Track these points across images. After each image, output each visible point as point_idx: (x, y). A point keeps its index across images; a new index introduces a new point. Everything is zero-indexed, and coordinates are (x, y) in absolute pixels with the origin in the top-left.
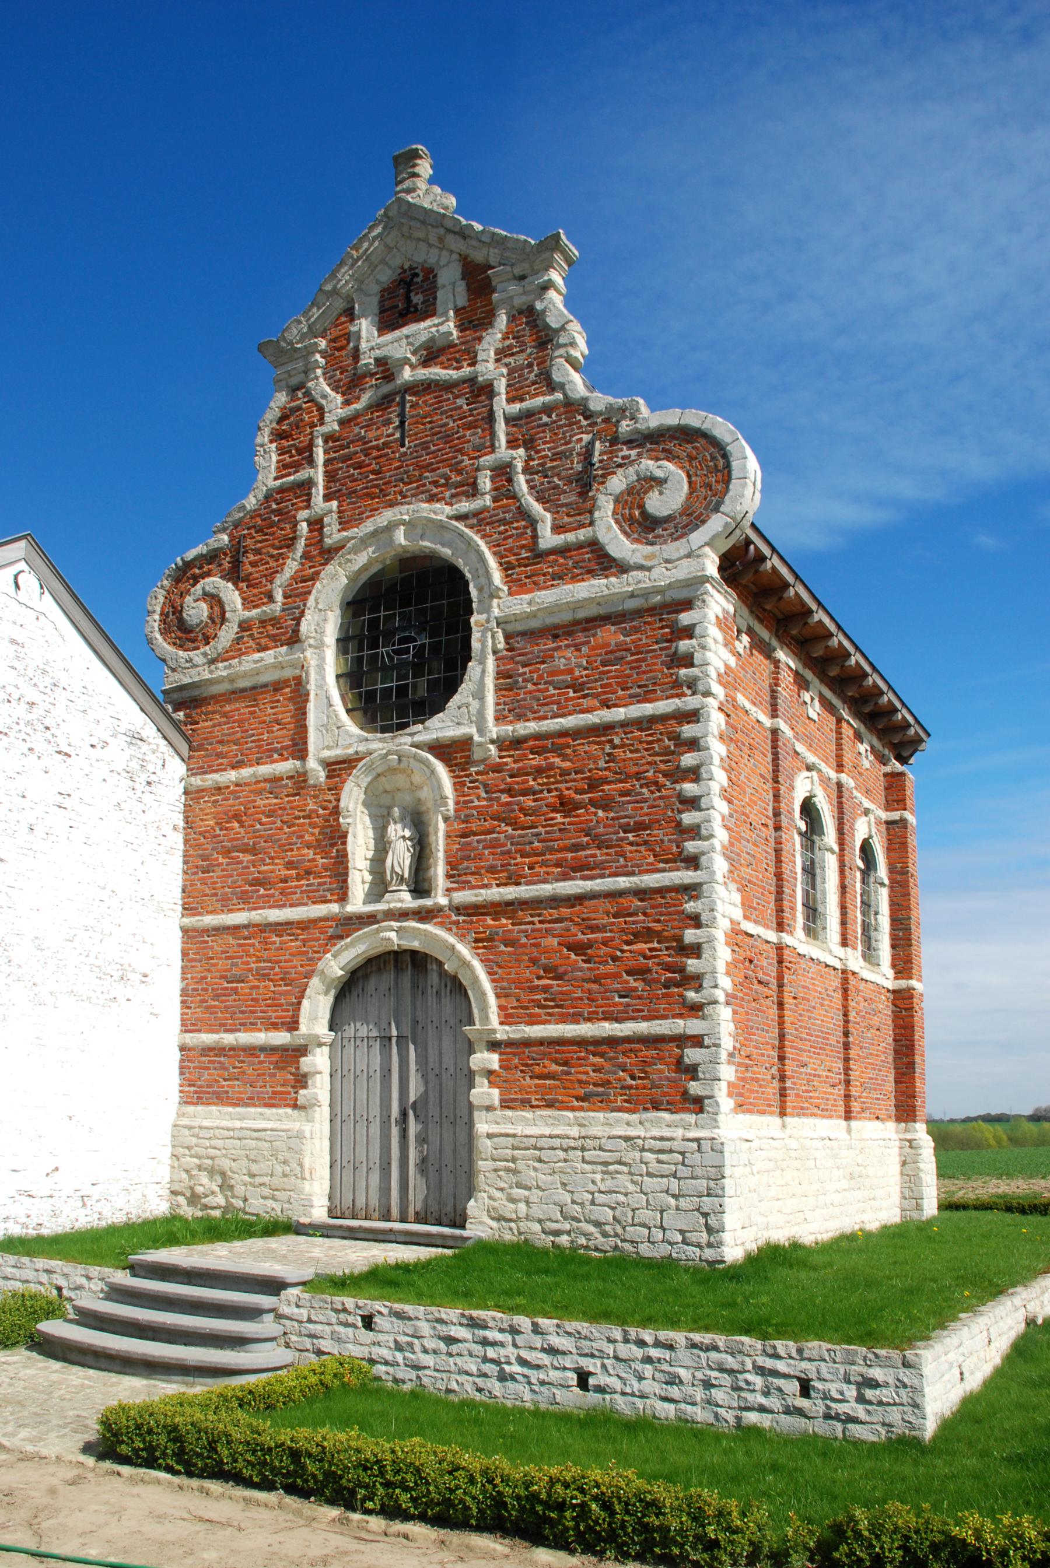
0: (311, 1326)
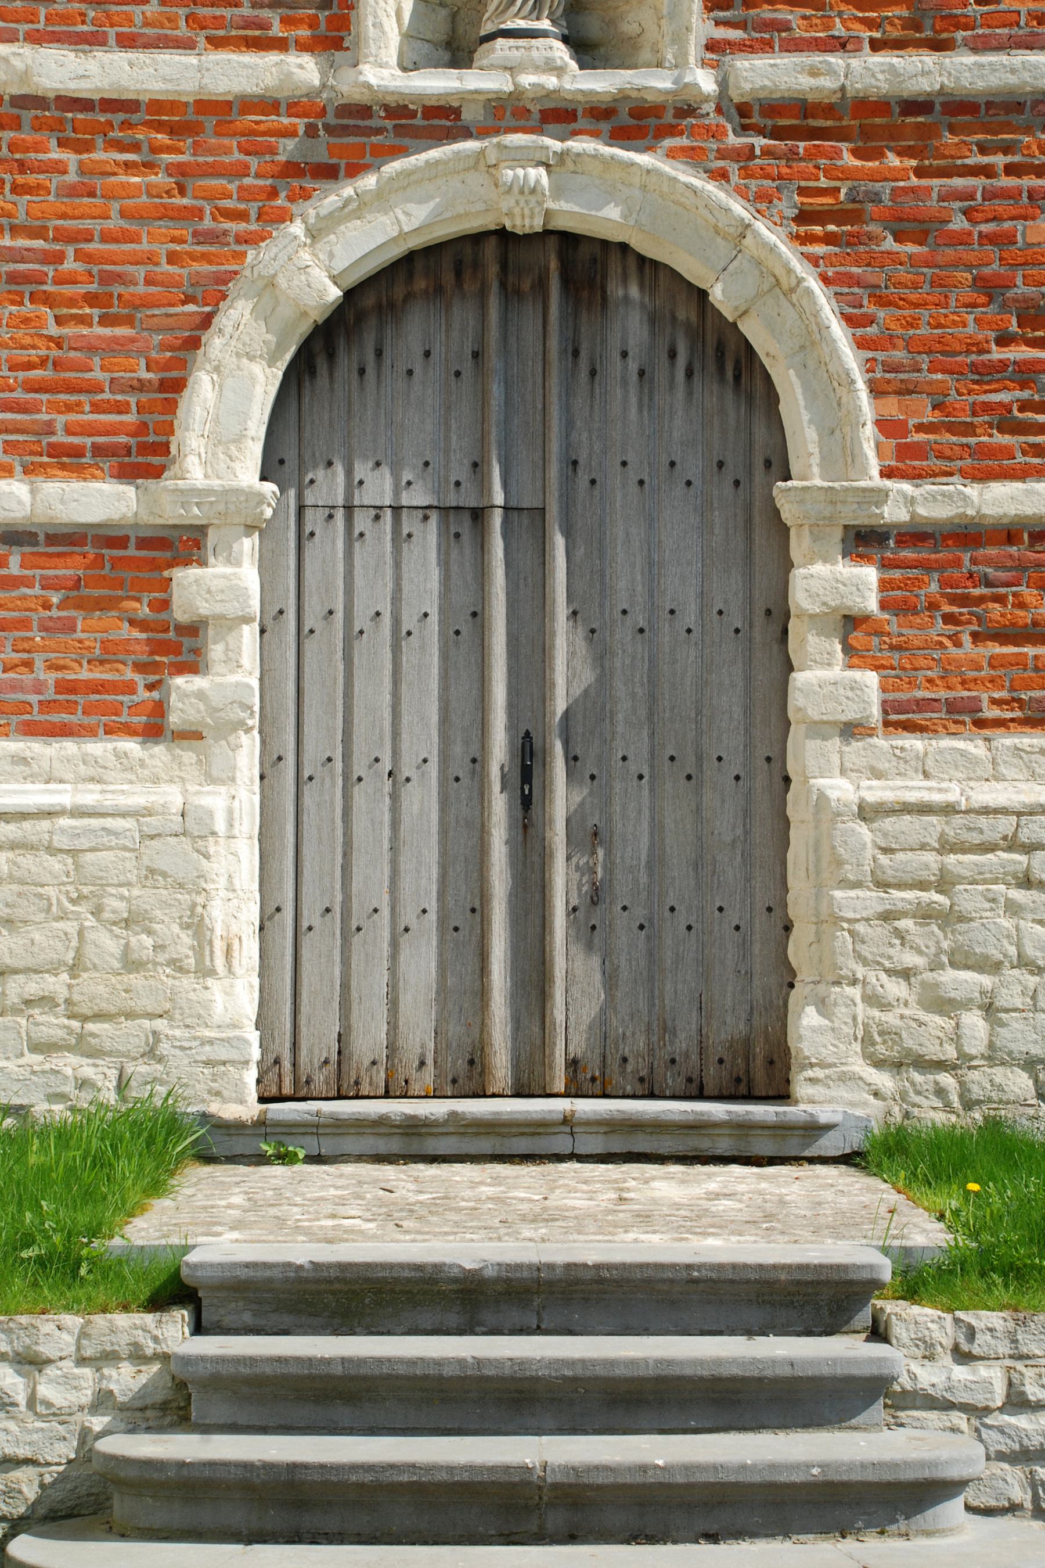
0: (1022, 1421)
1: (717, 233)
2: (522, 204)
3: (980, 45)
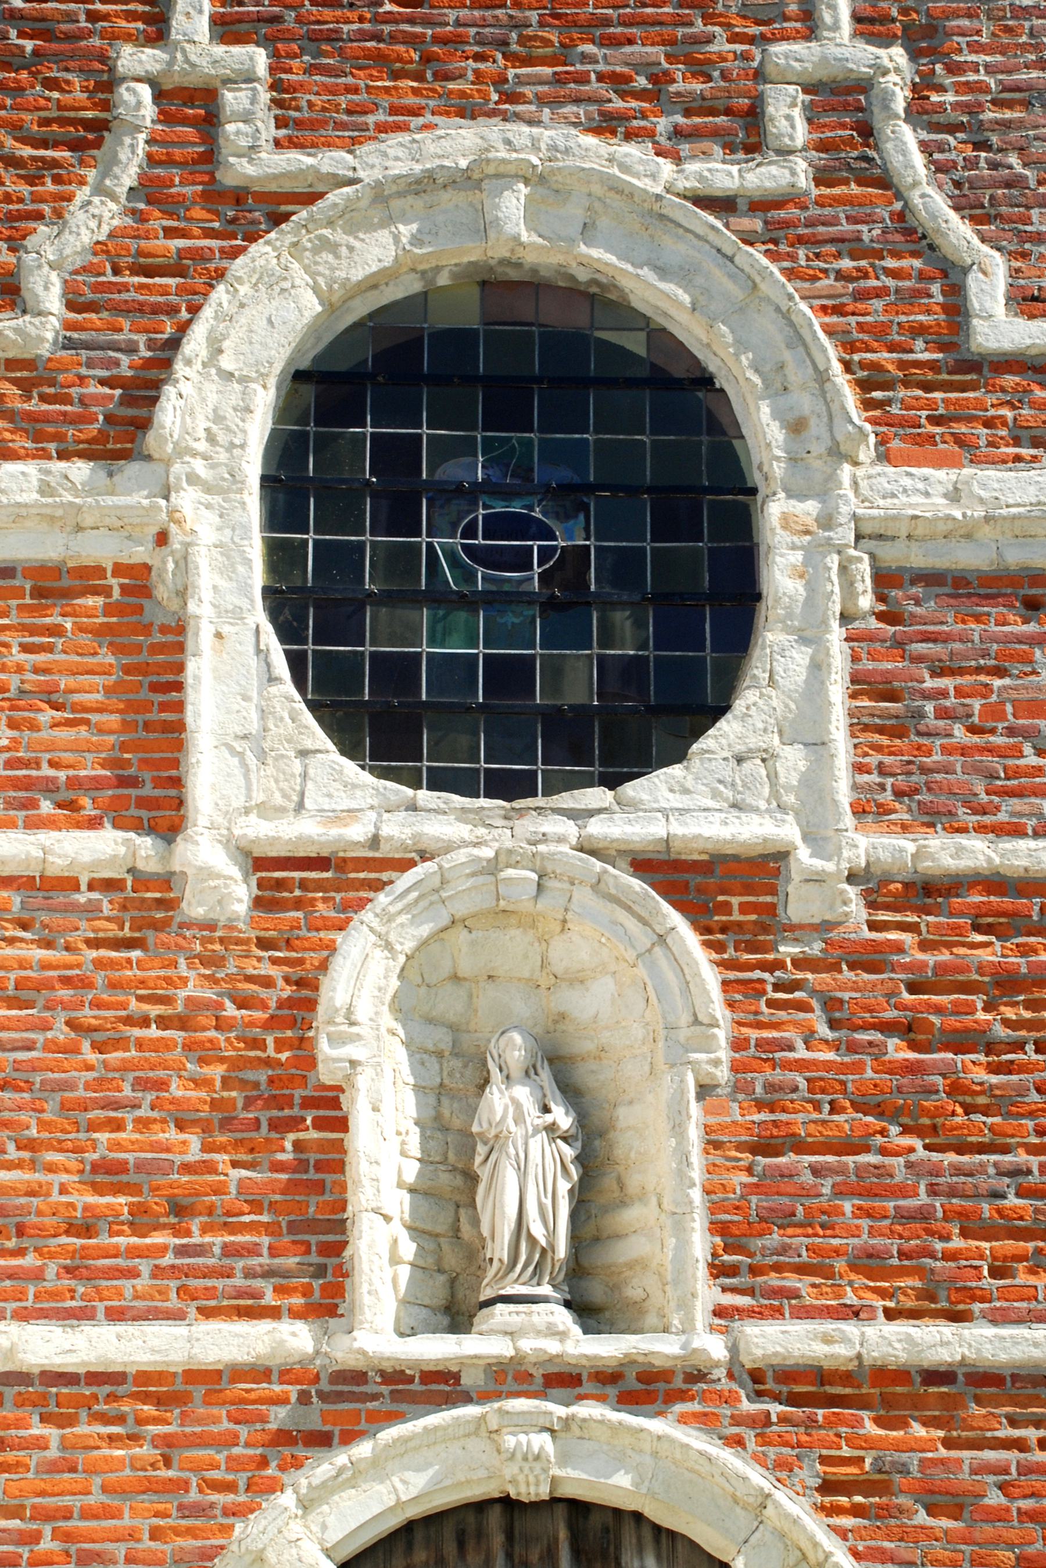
1: (736, 1502)
2: (526, 1471)
3: (998, 1318)
